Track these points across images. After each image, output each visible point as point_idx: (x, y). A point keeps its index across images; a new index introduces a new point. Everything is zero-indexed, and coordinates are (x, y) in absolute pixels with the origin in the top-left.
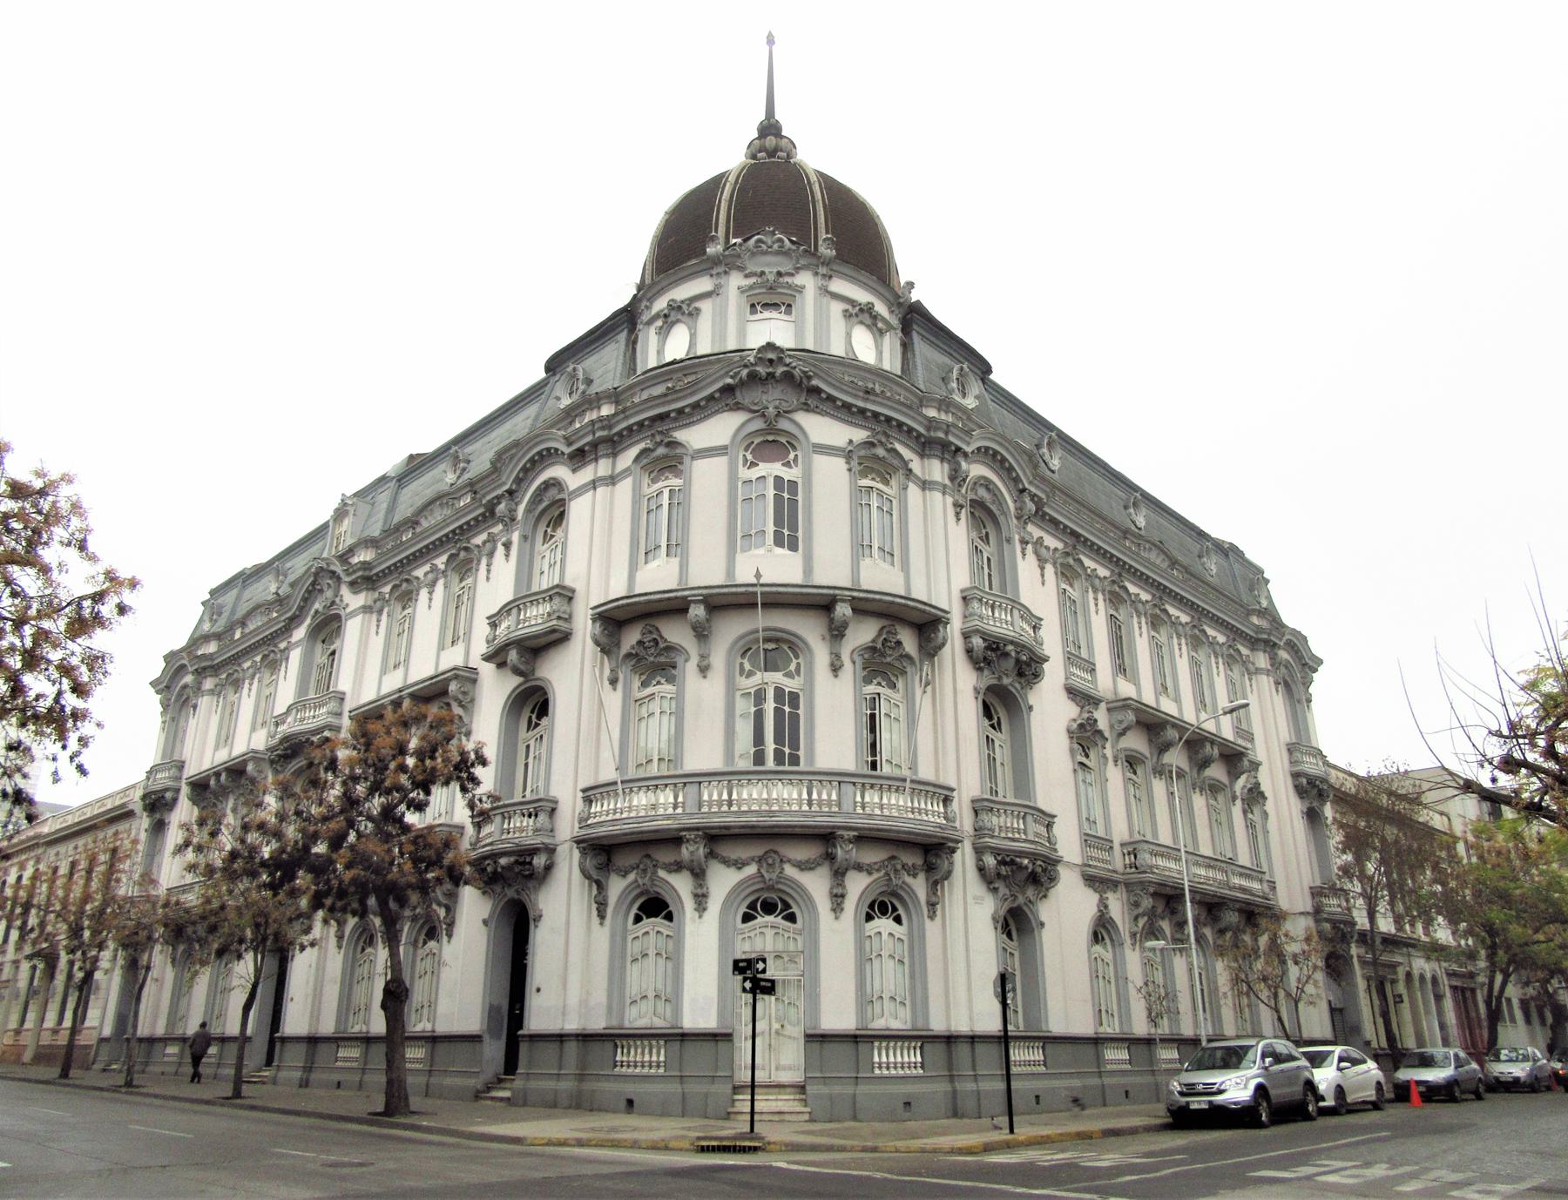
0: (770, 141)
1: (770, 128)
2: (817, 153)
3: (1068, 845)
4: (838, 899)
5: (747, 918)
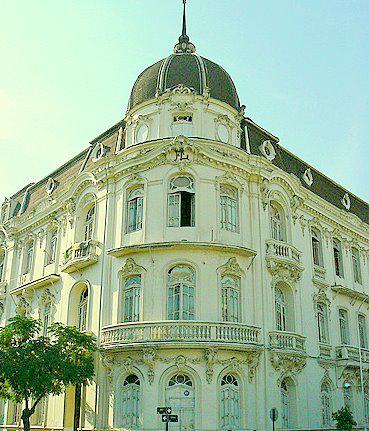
0: (184, 46)
1: (184, 39)
2: (203, 50)
3: (312, 348)
4: (209, 375)
5: (171, 384)
